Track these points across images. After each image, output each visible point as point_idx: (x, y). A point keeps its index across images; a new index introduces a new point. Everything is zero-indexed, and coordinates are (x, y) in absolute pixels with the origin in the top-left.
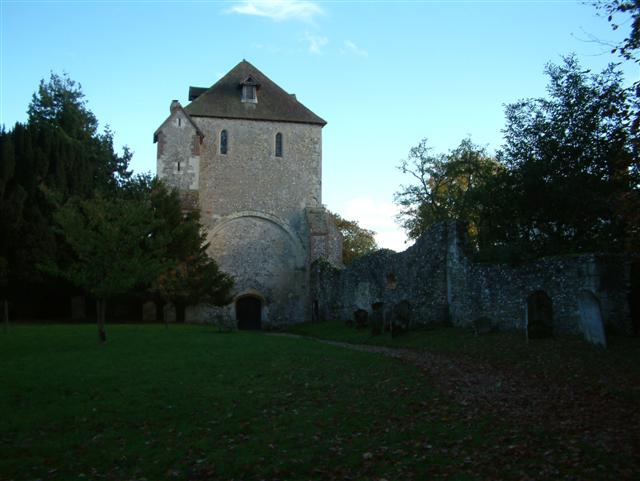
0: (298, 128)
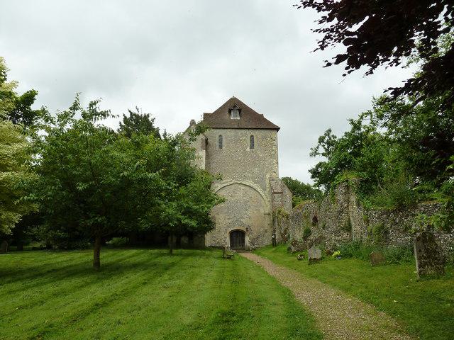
0: (263, 133)
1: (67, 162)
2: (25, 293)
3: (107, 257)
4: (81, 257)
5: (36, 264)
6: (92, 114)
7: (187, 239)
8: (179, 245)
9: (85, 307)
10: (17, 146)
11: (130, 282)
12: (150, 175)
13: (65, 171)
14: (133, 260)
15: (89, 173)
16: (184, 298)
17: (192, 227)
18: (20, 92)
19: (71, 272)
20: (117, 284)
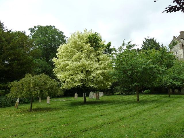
1: (123, 65)
2: (116, 108)
3: (142, 97)
4: (133, 97)
5: (118, 100)
6: (129, 46)
7: (178, 90)
8: (173, 93)
9: (134, 113)
10: (108, 61)
11: (150, 107)
12: (154, 66)
13: (123, 68)
14: (152, 99)
15: (131, 67)
16: (171, 114)
17: (178, 85)
18: (106, 44)
19: (129, 102)
20: (146, 107)
